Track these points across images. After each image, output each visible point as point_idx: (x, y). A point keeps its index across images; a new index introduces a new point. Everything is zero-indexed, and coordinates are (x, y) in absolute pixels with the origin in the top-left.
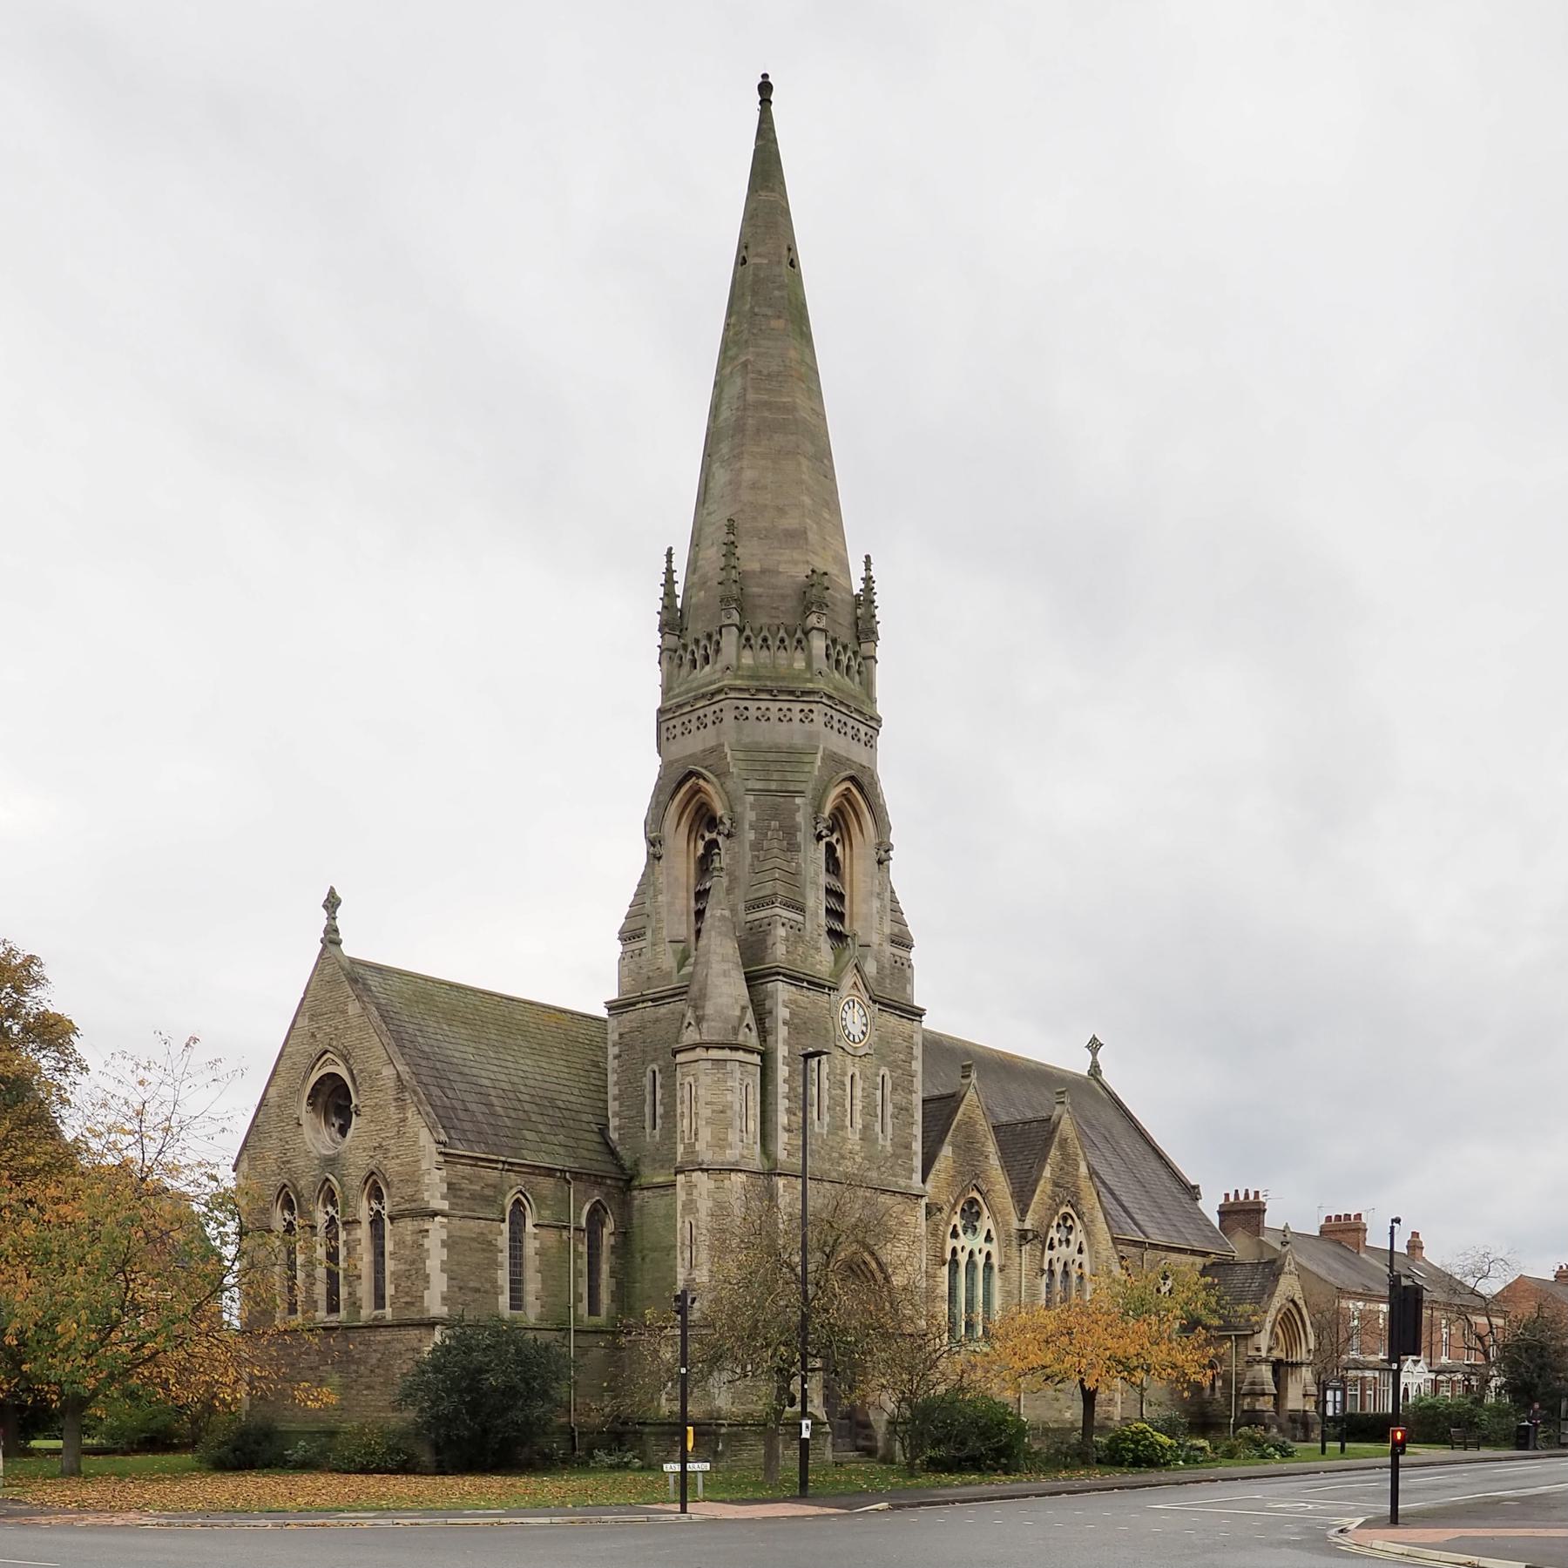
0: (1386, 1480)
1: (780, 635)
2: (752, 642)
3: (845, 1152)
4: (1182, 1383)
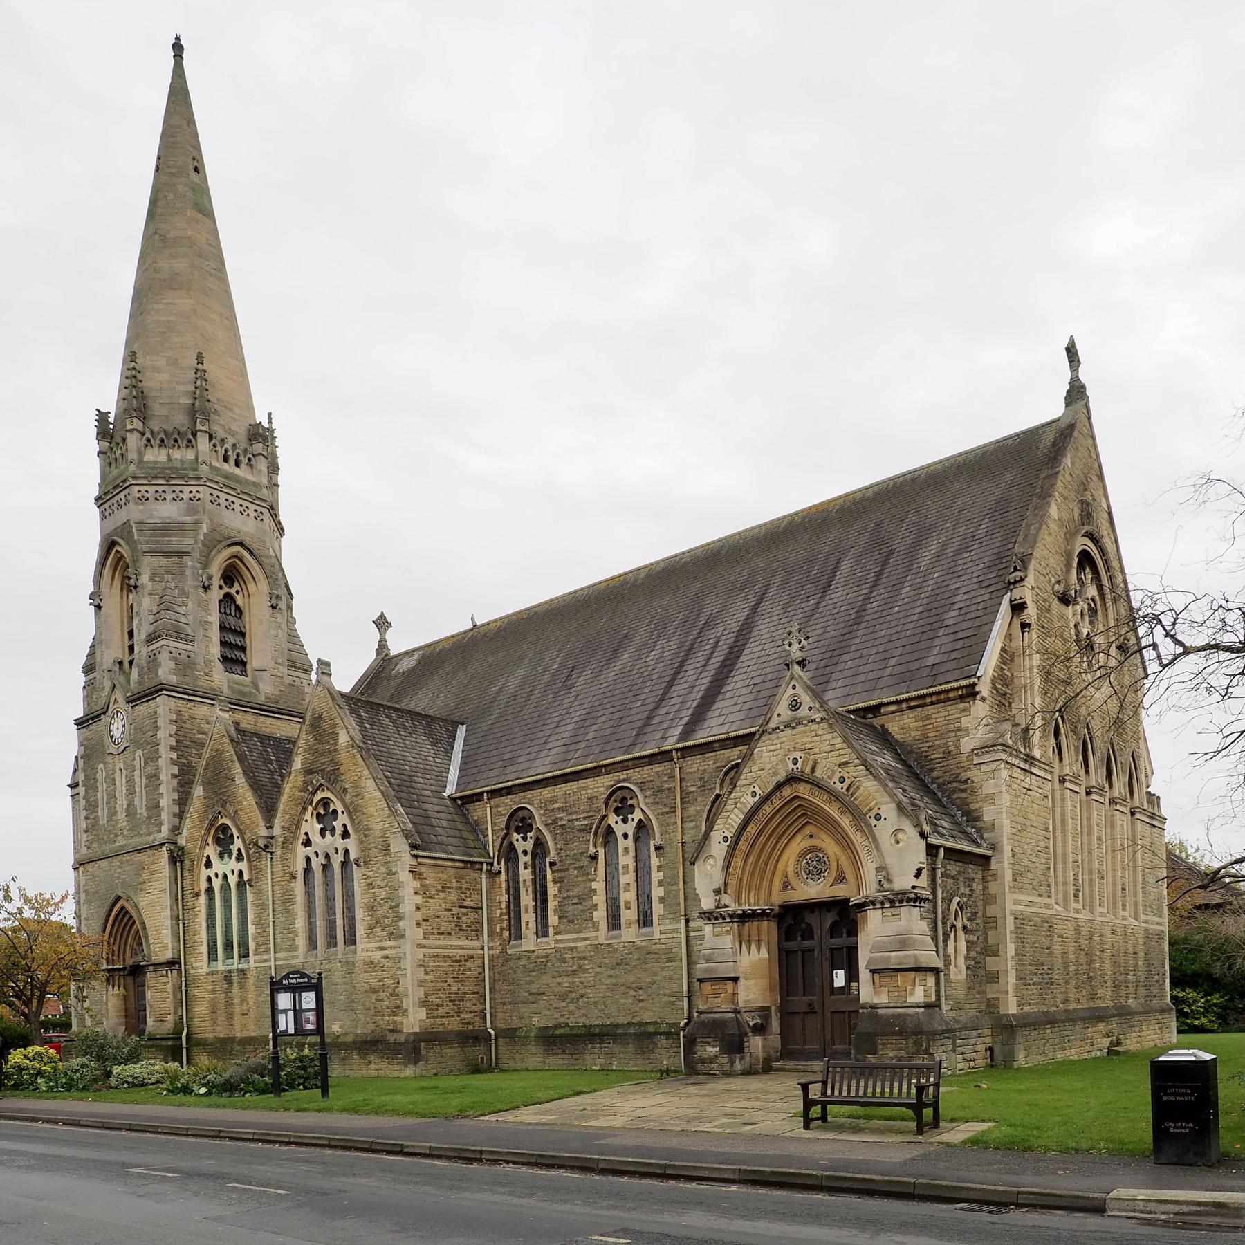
1: (160, 436)
2: (180, 442)
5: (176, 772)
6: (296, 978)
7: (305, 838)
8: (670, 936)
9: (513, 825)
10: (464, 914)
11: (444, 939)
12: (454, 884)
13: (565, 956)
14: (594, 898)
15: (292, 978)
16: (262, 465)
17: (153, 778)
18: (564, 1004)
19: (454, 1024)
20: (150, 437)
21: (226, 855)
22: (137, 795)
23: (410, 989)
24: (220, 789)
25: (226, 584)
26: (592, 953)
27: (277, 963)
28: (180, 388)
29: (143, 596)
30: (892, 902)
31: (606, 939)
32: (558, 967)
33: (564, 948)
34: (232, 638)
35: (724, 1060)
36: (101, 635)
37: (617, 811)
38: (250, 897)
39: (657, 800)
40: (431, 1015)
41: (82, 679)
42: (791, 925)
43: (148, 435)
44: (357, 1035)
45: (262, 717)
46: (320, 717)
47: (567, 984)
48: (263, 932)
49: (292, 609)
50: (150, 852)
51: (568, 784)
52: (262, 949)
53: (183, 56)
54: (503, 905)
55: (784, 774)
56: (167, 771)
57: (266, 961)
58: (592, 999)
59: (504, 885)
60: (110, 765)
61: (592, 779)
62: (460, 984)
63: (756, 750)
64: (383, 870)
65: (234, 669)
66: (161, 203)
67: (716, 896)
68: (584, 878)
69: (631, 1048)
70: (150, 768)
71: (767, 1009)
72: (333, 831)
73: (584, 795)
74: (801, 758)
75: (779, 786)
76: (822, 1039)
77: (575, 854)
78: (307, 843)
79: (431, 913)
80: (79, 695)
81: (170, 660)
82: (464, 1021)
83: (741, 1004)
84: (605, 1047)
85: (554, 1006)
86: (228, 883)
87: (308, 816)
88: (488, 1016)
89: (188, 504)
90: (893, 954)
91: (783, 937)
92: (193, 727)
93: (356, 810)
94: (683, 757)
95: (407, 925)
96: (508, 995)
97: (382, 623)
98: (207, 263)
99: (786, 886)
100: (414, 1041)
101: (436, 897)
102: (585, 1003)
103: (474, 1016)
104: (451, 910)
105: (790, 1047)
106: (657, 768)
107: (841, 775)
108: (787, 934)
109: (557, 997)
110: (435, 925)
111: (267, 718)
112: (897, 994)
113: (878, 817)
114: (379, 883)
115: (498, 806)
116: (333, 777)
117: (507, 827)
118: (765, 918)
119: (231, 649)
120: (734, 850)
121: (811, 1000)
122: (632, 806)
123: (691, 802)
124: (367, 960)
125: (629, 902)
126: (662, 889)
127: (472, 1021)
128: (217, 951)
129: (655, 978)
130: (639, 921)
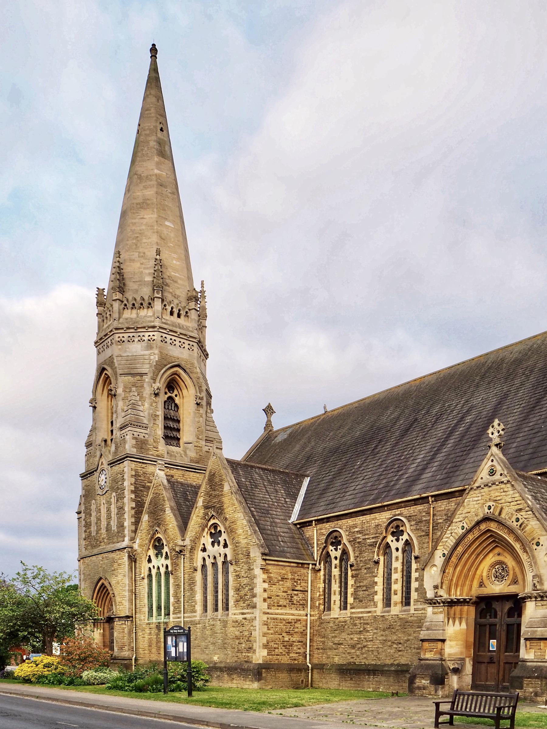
0: (431, 711)
3: (101, 539)
5: (134, 506)
6: (177, 630)
7: (203, 547)
8: (420, 612)
9: (330, 540)
11: (281, 609)
13: (357, 622)
14: (376, 587)
15: (175, 630)
16: (193, 315)
17: (121, 509)
18: (353, 651)
19: (285, 660)
20: (126, 303)
21: (159, 556)
22: (112, 519)
23: (257, 638)
24: (157, 516)
25: (169, 391)
26: (372, 621)
27: (185, 619)
28: (147, 271)
29: (119, 401)
30: (542, 597)
31: (381, 613)
32: (352, 629)
33: (356, 617)
34: (171, 424)
35: (432, 688)
36: (95, 424)
37: (393, 534)
38: (171, 581)
39: (418, 527)
40: (271, 654)
41: (84, 450)
42: (484, 609)
43: (125, 302)
44: (228, 663)
45: (188, 472)
46: (214, 475)
47: (356, 639)
48: (178, 601)
49: (210, 404)
50: (118, 552)
51: (364, 516)
52: (177, 611)
53: (157, 56)
54: (321, 590)
55: (482, 516)
56: (128, 505)
57: (179, 618)
58: (371, 649)
59: (322, 578)
60: (98, 501)
61: (379, 514)
62: (290, 636)
63: (466, 500)
64: (246, 567)
65: (172, 443)
67: (435, 590)
68: (371, 575)
69: (391, 679)
70: (119, 504)
71: (463, 659)
72: (219, 543)
73: (373, 523)
74: (493, 505)
75: (478, 523)
76: (497, 679)
77: (366, 560)
78: (204, 550)
79: (274, 593)
80: (83, 459)
81: (133, 439)
82: (292, 658)
83: (446, 656)
84: (376, 678)
85: (348, 652)
86: (160, 572)
88: (308, 656)
89: (148, 343)
90: (539, 629)
91: (479, 616)
92: (145, 479)
93: (231, 531)
94: (436, 501)
95: (258, 600)
96: (321, 644)
97: (269, 410)
98: (166, 190)
99: (481, 584)
100: (258, 668)
101: (277, 584)
102: (366, 651)
103: (299, 655)
105: (477, 683)
106: (419, 507)
107: (517, 517)
108: (481, 614)
109: (350, 646)
110: (275, 601)
111: (190, 473)
112: (540, 654)
113: (538, 544)
114: (243, 575)
115: (321, 529)
116: (220, 511)
117: (326, 542)
118: (466, 604)
119: (171, 430)
120: (448, 562)
121: (491, 655)
122: (402, 531)
123: (439, 529)
124: (235, 620)
125: (397, 591)
126: (417, 583)
127: (297, 658)
128: (152, 611)
129: (409, 638)
130: (402, 602)
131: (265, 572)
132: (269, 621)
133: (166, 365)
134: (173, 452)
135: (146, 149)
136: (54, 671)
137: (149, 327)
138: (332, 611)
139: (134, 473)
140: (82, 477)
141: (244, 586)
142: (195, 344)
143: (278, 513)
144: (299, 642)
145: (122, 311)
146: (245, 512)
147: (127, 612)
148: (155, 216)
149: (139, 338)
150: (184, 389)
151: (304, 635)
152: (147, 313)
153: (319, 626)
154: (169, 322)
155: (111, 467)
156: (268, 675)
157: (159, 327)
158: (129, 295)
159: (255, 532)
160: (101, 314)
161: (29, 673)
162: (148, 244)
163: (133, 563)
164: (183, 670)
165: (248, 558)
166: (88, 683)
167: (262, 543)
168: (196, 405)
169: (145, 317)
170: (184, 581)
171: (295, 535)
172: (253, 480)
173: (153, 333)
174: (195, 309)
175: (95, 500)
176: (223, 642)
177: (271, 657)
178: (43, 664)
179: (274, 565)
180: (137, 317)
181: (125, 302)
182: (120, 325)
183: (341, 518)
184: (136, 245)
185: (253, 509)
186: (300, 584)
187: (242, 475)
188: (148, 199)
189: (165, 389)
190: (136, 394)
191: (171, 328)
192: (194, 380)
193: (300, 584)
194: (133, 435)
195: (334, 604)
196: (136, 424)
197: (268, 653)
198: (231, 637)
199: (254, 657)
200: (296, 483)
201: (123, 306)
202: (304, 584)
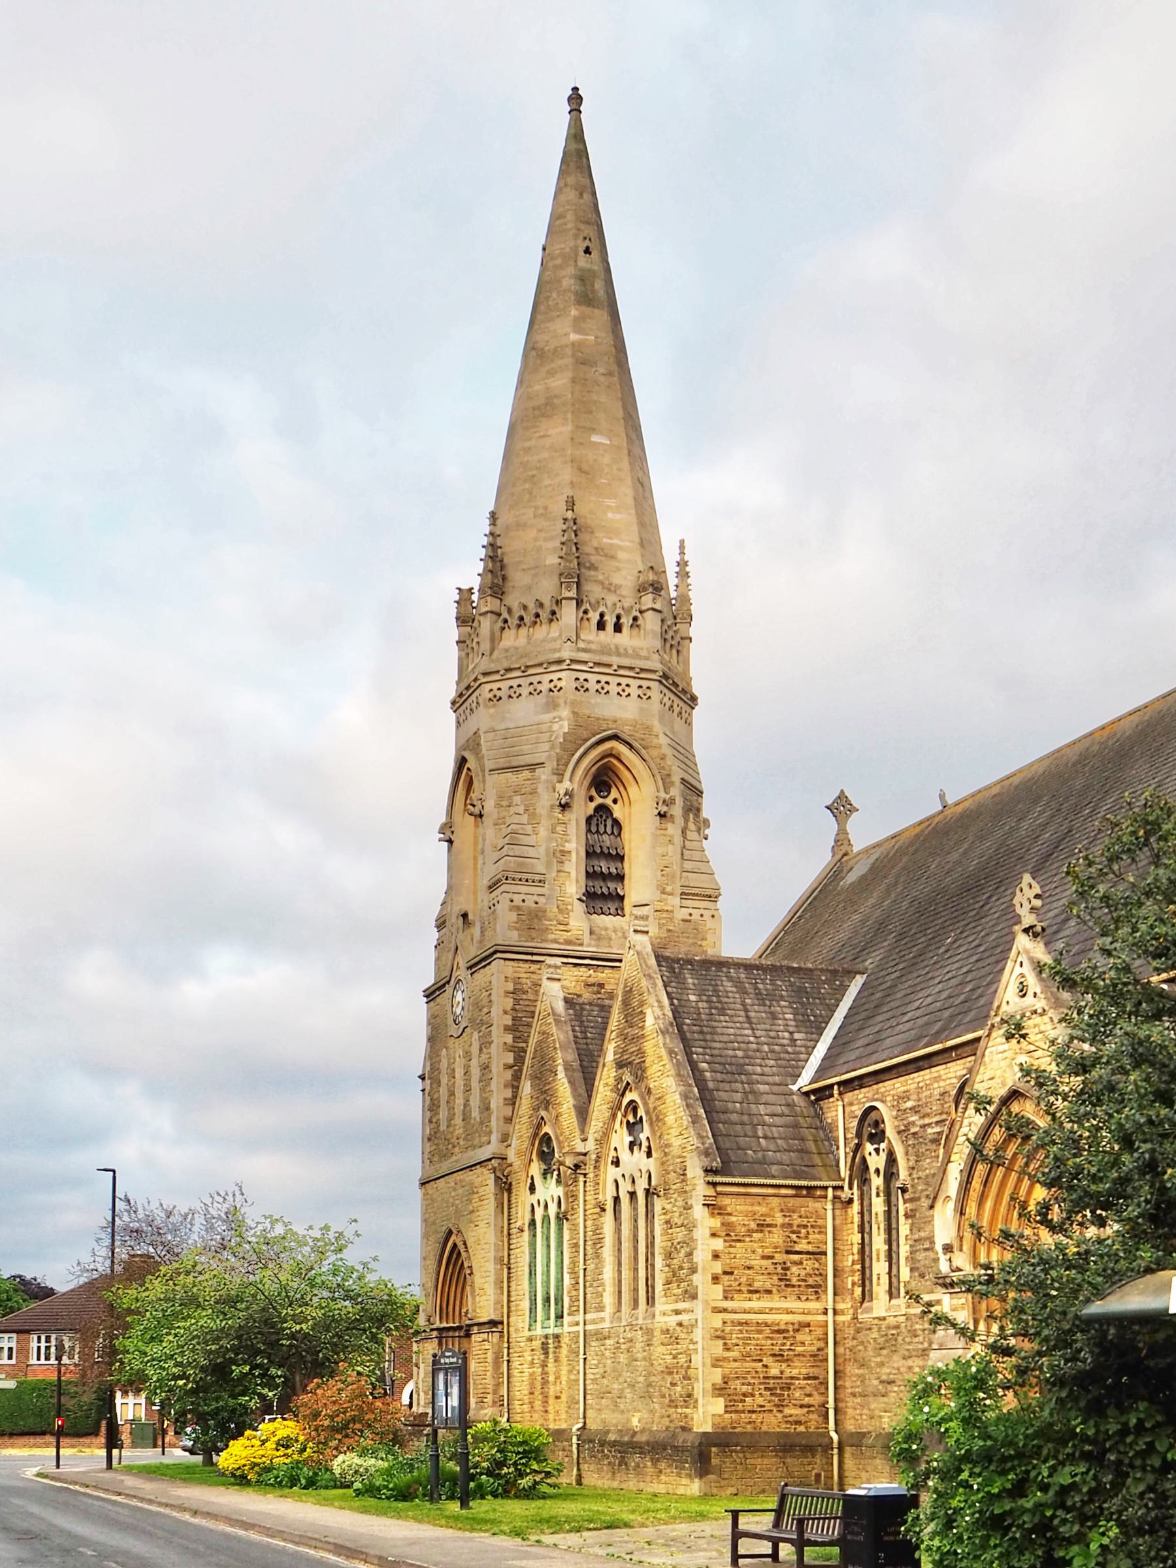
4: (1053, 1280)
10: (795, 1263)
11: (759, 1299)
12: (779, 1219)
19: (772, 1423)
23: (700, 1370)
24: (544, 1086)
27: (588, 1327)
32: (909, 1343)
34: (604, 866)
40: (733, 1409)
43: (505, 615)
54: (856, 1249)
56: (500, 1058)
61: (944, 1066)
62: (784, 1365)
64: (680, 1203)
65: (605, 909)
66: (542, 308)
77: (927, 1176)
78: (616, 1163)
79: (738, 1262)
82: (789, 1419)
86: (548, 1216)
87: (617, 1125)
89: (548, 696)
95: (700, 1280)
97: (841, 808)
101: (747, 1239)
103: (808, 1412)
104: (772, 1257)
110: (743, 1280)
115: (851, 1104)
116: (640, 1073)
117: (859, 1134)
127: (803, 1419)
131: (716, 1211)
132: (728, 1329)
133: (586, 740)
134: (606, 929)
135: (554, 295)
136: (295, 1457)
137: (550, 663)
138: (874, 1301)
139: (510, 987)
140: (427, 996)
141: (678, 1247)
142: (655, 685)
143: (767, 1070)
144: (809, 1378)
145: (497, 634)
146: (679, 1075)
147: (492, 1311)
148: (570, 428)
149: (531, 689)
150: (631, 785)
151: (821, 1361)
152: (548, 634)
153: (854, 1338)
154: (593, 647)
155: (472, 974)
156: (725, 1463)
157: (571, 660)
158: (514, 599)
159: (695, 1120)
160: (464, 642)
161: (243, 1462)
162: (554, 489)
163: (506, 1195)
164: (496, 1449)
165: (683, 1181)
166: (341, 1483)
167: (707, 1145)
168: (658, 817)
169: (543, 641)
170: (585, 1236)
171: (801, 1120)
172: (718, 996)
173: (559, 675)
174: (653, 609)
175: (447, 1048)
176: (645, 1380)
177: (733, 1415)
178: (276, 1439)
179: (738, 1194)
180: (529, 643)
181: (505, 615)
182: (492, 665)
183: (882, 1077)
184: (531, 493)
185: (705, 1065)
186: (807, 1238)
187: (691, 986)
188: (556, 396)
189: (589, 788)
190: (521, 810)
191: (597, 659)
192: (653, 765)
193: (807, 1238)
194: (512, 901)
195: (878, 1284)
196: (518, 876)
197: (726, 1406)
198: (660, 1369)
199: (695, 1416)
200: (828, 993)
201: (500, 624)
202: (817, 1236)
